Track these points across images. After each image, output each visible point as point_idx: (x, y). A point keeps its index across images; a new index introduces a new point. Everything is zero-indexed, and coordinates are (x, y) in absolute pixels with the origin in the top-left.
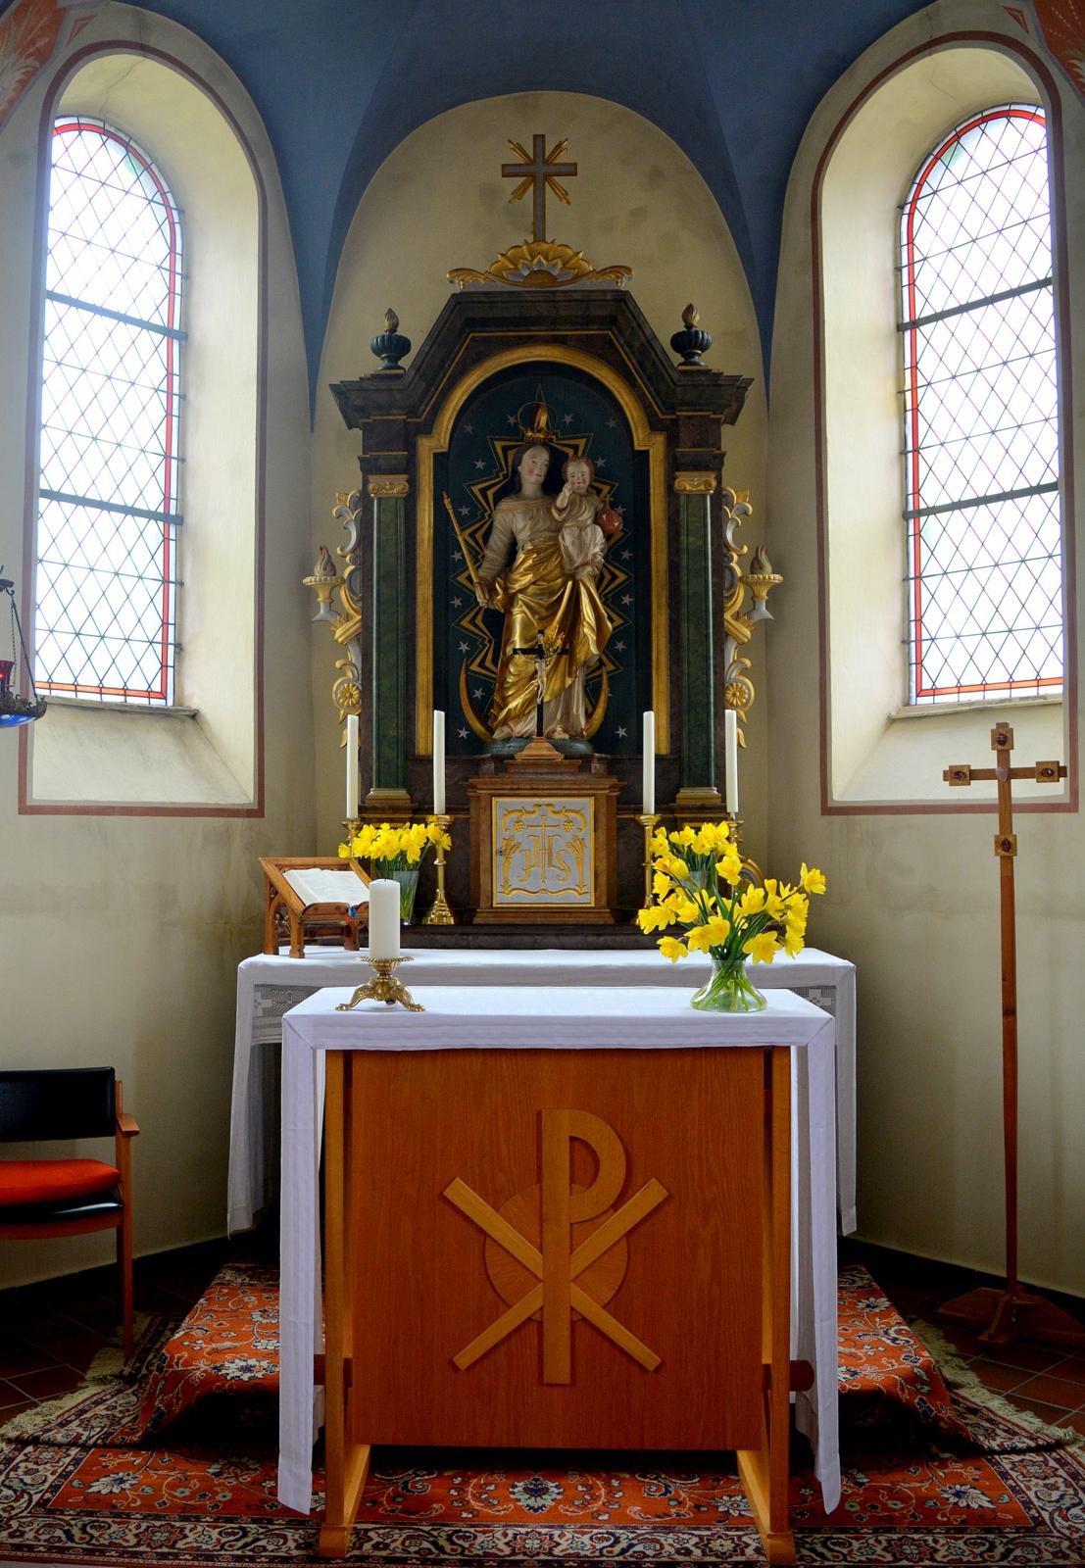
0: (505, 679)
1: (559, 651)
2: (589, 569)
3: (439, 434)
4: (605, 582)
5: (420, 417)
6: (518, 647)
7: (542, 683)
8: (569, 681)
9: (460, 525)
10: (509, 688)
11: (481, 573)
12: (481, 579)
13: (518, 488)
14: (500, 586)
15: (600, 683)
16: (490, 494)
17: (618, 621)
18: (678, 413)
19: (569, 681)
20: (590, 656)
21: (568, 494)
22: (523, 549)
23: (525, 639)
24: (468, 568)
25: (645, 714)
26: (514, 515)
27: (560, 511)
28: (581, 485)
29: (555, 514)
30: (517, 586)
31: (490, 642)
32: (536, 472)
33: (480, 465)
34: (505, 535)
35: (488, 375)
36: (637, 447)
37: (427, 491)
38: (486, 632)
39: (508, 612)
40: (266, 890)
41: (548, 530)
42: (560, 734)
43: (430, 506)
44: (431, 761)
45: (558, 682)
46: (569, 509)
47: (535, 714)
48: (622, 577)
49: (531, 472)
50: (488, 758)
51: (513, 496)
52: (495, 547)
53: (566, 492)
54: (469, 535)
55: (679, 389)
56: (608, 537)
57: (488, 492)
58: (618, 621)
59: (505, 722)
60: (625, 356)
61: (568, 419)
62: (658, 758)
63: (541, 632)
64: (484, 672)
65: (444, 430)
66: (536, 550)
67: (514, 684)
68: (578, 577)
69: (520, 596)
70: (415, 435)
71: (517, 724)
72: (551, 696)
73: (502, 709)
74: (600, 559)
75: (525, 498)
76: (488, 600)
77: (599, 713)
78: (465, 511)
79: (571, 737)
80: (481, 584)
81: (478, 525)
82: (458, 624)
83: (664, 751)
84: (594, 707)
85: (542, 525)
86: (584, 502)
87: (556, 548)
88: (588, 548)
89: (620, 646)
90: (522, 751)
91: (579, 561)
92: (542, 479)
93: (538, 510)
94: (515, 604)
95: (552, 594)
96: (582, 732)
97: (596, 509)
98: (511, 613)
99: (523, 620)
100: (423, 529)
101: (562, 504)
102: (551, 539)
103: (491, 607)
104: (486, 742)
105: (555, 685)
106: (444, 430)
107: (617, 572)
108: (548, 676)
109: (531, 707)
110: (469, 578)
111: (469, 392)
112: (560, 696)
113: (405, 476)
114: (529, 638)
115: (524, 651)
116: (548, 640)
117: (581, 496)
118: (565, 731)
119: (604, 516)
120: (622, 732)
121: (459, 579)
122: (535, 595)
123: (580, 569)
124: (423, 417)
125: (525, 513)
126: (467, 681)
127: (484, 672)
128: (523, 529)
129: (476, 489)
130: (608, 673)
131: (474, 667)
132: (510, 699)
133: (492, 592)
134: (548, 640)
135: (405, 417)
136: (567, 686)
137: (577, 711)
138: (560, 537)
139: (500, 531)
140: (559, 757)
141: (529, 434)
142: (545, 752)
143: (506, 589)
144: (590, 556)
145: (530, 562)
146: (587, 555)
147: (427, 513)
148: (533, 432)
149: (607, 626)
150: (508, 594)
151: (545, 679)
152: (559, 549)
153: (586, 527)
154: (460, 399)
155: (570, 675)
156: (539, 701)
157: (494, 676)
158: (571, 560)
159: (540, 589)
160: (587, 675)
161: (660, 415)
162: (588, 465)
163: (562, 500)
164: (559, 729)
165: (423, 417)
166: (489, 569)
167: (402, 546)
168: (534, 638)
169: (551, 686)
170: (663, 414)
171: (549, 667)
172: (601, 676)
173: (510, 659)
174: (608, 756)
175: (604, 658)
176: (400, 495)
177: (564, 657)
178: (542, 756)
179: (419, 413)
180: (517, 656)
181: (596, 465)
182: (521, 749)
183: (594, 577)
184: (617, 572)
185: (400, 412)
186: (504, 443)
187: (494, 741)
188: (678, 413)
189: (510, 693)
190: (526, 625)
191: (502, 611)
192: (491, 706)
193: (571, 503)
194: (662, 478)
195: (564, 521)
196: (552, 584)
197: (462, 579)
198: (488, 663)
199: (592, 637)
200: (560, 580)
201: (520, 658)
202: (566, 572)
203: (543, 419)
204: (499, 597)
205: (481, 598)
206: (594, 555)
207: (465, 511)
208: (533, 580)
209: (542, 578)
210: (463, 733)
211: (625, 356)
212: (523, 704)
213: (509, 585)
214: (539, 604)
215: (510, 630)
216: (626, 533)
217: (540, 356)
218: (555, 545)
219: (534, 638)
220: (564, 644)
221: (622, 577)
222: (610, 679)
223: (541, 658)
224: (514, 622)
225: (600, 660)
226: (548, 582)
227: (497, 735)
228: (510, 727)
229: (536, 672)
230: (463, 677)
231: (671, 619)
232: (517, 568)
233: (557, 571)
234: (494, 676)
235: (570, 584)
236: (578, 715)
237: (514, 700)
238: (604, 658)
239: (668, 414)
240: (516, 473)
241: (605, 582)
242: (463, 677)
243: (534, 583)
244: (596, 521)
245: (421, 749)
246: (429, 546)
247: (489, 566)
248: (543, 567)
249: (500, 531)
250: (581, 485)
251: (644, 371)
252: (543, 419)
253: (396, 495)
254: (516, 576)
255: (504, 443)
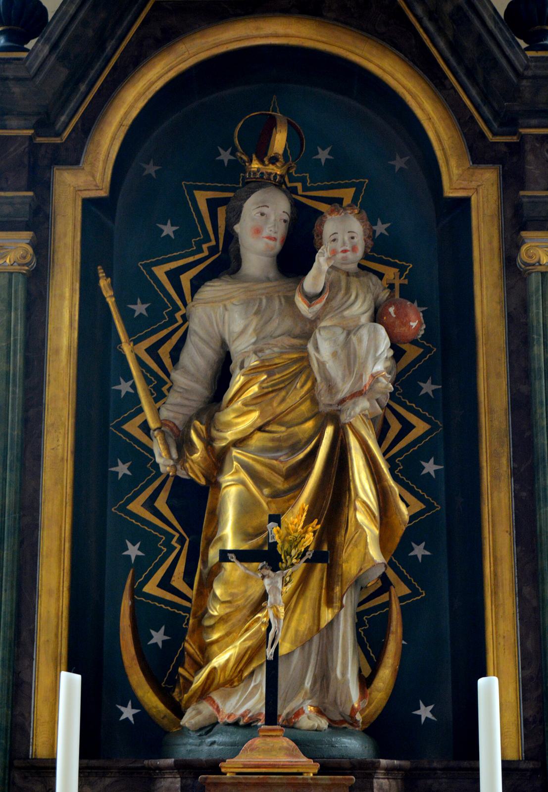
0: (206, 611)
1: (309, 555)
2: (363, 404)
3: (93, 165)
4: (391, 435)
5: (59, 135)
6: (230, 546)
7: (277, 617)
8: (327, 615)
9: (130, 333)
10: (212, 627)
11: (165, 414)
12: (163, 423)
13: (233, 265)
14: (199, 435)
15: (386, 619)
16: (186, 280)
17: (418, 506)
18: (523, 131)
19: (327, 615)
20: (367, 566)
21: (325, 267)
22: (242, 367)
23: (242, 532)
24: (141, 410)
25: (481, 682)
26: (226, 308)
27: (311, 299)
28: (350, 255)
29: (301, 304)
30: (230, 435)
31: (181, 541)
32: (266, 232)
33: (168, 230)
34: (211, 347)
35: (184, 66)
36: (449, 192)
37: (68, 263)
38: (175, 523)
39: (213, 485)
40: (231, 729)
41: (289, 334)
42: (311, 720)
43: (72, 290)
44: (54, 768)
45: (306, 616)
46: (326, 296)
47: (261, 678)
48: (420, 427)
49: (258, 231)
50: (169, 768)
51: (226, 278)
52: (192, 369)
53: (322, 262)
54: (146, 350)
55: (525, 83)
56: (398, 352)
57: (182, 277)
58: (418, 506)
59: (204, 693)
60: (424, 36)
61: (323, 155)
62: (508, 768)
63: (275, 518)
64: (169, 596)
65: (102, 157)
66: (266, 367)
67: (222, 619)
68: (344, 418)
69: (235, 452)
70: (49, 167)
71: (227, 697)
72: (293, 643)
73: (199, 667)
74: (386, 384)
75: (245, 280)
76: (177, 461)
77: (386, 675)
78: (140, 308)
79: (332, 724)
80: (163, 432)
81: (165, 332)
82: (123, 509)
83: (513, 755)
84: (375, 667)
85: (280, 324)
86: (355, 283)
87: (303, 365)
88: (364, 365)
89: (419, 551)
90: (235, 754)
91: (345, 388)
92: (277, 246)
93: (270, 299)
94: (226, 468)
95: (295, 448)
96: (352, 716)
97: (375, 300)
98: (217, 486)
99: (239, 495)
100: (58, 330)
101: (315, 284)
102: (293, 348)
103: (182, 474)
104: (167, 733)
105: (302, 621)
106: (102, 157)
107: (412, 418)
108: (287, 605)
109: (254, 665)
110: (145, 427)
111: (150, 94)
112: (310, 641)
113: (27, 235)
114: (250, 530)
115: (242, 556)
116: (288, 534)
117: (348, 274)
118: (321, 712)
119: (392, 310)
120: (425, 712)
121: (126, 427)
122: (263, 450)
123: (349, 404)
124: (66, 134)
125: (247, 303)
126: (133, 608)
127: (169, 596)
128: (243, 332)
129: (160, 272)
130: (401, 599)
131: (151, 588)
132: (215, 648)
133: (183, 445)
134: (288, 534)
135: (30, 132)
136: (323, 624)
137: (344, 674)
138: (310, 347)
139: (201, 338)
140: (309, 768)
141: (255, 165)
142: (283, 759)
143: (209, 441)
144: (366, 379)
145: (254, 389)
146: (361, 377)
147: (67, 303)
148: (262, 161)
149: (399, 510)
150: (213, 448)
151: (282, 610)
152: (309, 366)
153: (359, 327)
154: (132, 107)
155: (330, 603)
156: (269, 652)
157: (187, 604)
158: (331, 387)
159: (273, 440)
160: (360, 604)
161: (489, 135)
162: (360, 220)
163: (313, 281)
164: (309, 709)
165: (66, 134)
166: (182, 406)
167: (19, 360)
168: (260, 531)
169: (293, 624)
170: (495, 134)
171: (290, 586)
172: (388, 604)
173: (214, 572)
174: (405, 763)
175: (392, 575)
176: (16, 268)
177: (319, 566)
178: (273, 766)
179: (58, 126)
180: (227, 566)
181: (374, 232)
182: (235, 749)
183: (373, 420)
184: (412, 418)
185: (22, 123)
186: (211, 195)
187: (183, 731)
188: (523, 131)
189: (215, 636)
190: (246, 506)
191: (202, 482)
192: (181, 663)
193: (331, 286)
194: (496, 244)
195: (318, 318)
196: (296, 429)
197: (132, 427)
198: (177, 581)
199: (371, 531)
200: (310, 424)
201: (233, 570)
202: (322, 408)
203: (279, 141)
204: (196, 456)
205: (163, 457)
206: (375, 378)
207: (140, 308)
208: (260, 423)
209: (277, 420)
210: (128, 713)
211: (424, 36)
212: (240, 658)
213: (214, 433)
214: (272, 468)
215: (216, 518)
216: (427, 350)
217: (277, 36)
218: (301, 359)
219: (260, 531)
220: (319, 542)
221: (420, 427)
222: (404, 610)
223: (275, 569)
224: (224, 502)
225: (384, 577)
226: (288, 425)
227: (190, 719)
228: (213, 702)
229: (265, 596)
230: (126, 604)
231: (517, 497)
232: (231, 401)
233: (305, 407)
234: (187, 604)
235: (329, 431)
236: (345, 682)
237: (222, 650)
238: (392, 575)
239: (502, 134)
240: (231, 238)
241: (391, 435)
242: (126, 604)
243: (261, 429)
244: (377, 316)
245: (39, 750)
246: (69, 361)
247: (179, 400)
248: (279, 399)
249: (201, 338)
250: (350, 255)
251: (460, 60)
252: (279, 141)
253: (11, 269)
254: (228, 415)
255: (211, 195)
